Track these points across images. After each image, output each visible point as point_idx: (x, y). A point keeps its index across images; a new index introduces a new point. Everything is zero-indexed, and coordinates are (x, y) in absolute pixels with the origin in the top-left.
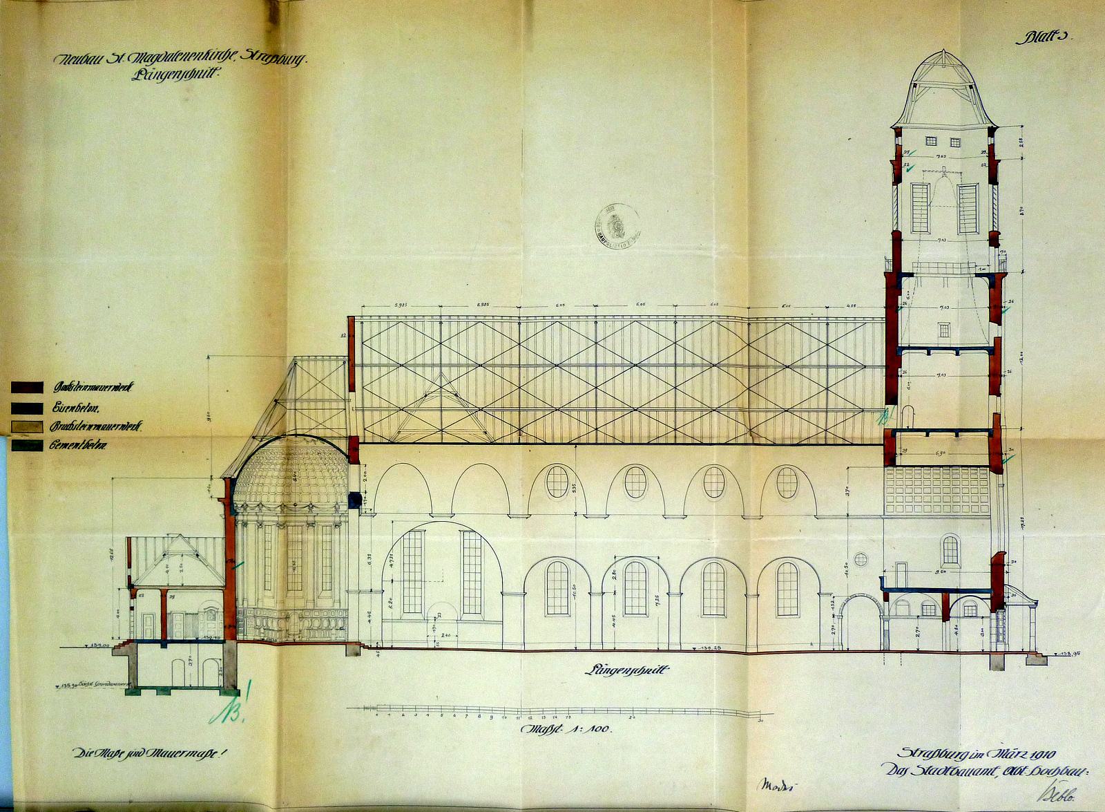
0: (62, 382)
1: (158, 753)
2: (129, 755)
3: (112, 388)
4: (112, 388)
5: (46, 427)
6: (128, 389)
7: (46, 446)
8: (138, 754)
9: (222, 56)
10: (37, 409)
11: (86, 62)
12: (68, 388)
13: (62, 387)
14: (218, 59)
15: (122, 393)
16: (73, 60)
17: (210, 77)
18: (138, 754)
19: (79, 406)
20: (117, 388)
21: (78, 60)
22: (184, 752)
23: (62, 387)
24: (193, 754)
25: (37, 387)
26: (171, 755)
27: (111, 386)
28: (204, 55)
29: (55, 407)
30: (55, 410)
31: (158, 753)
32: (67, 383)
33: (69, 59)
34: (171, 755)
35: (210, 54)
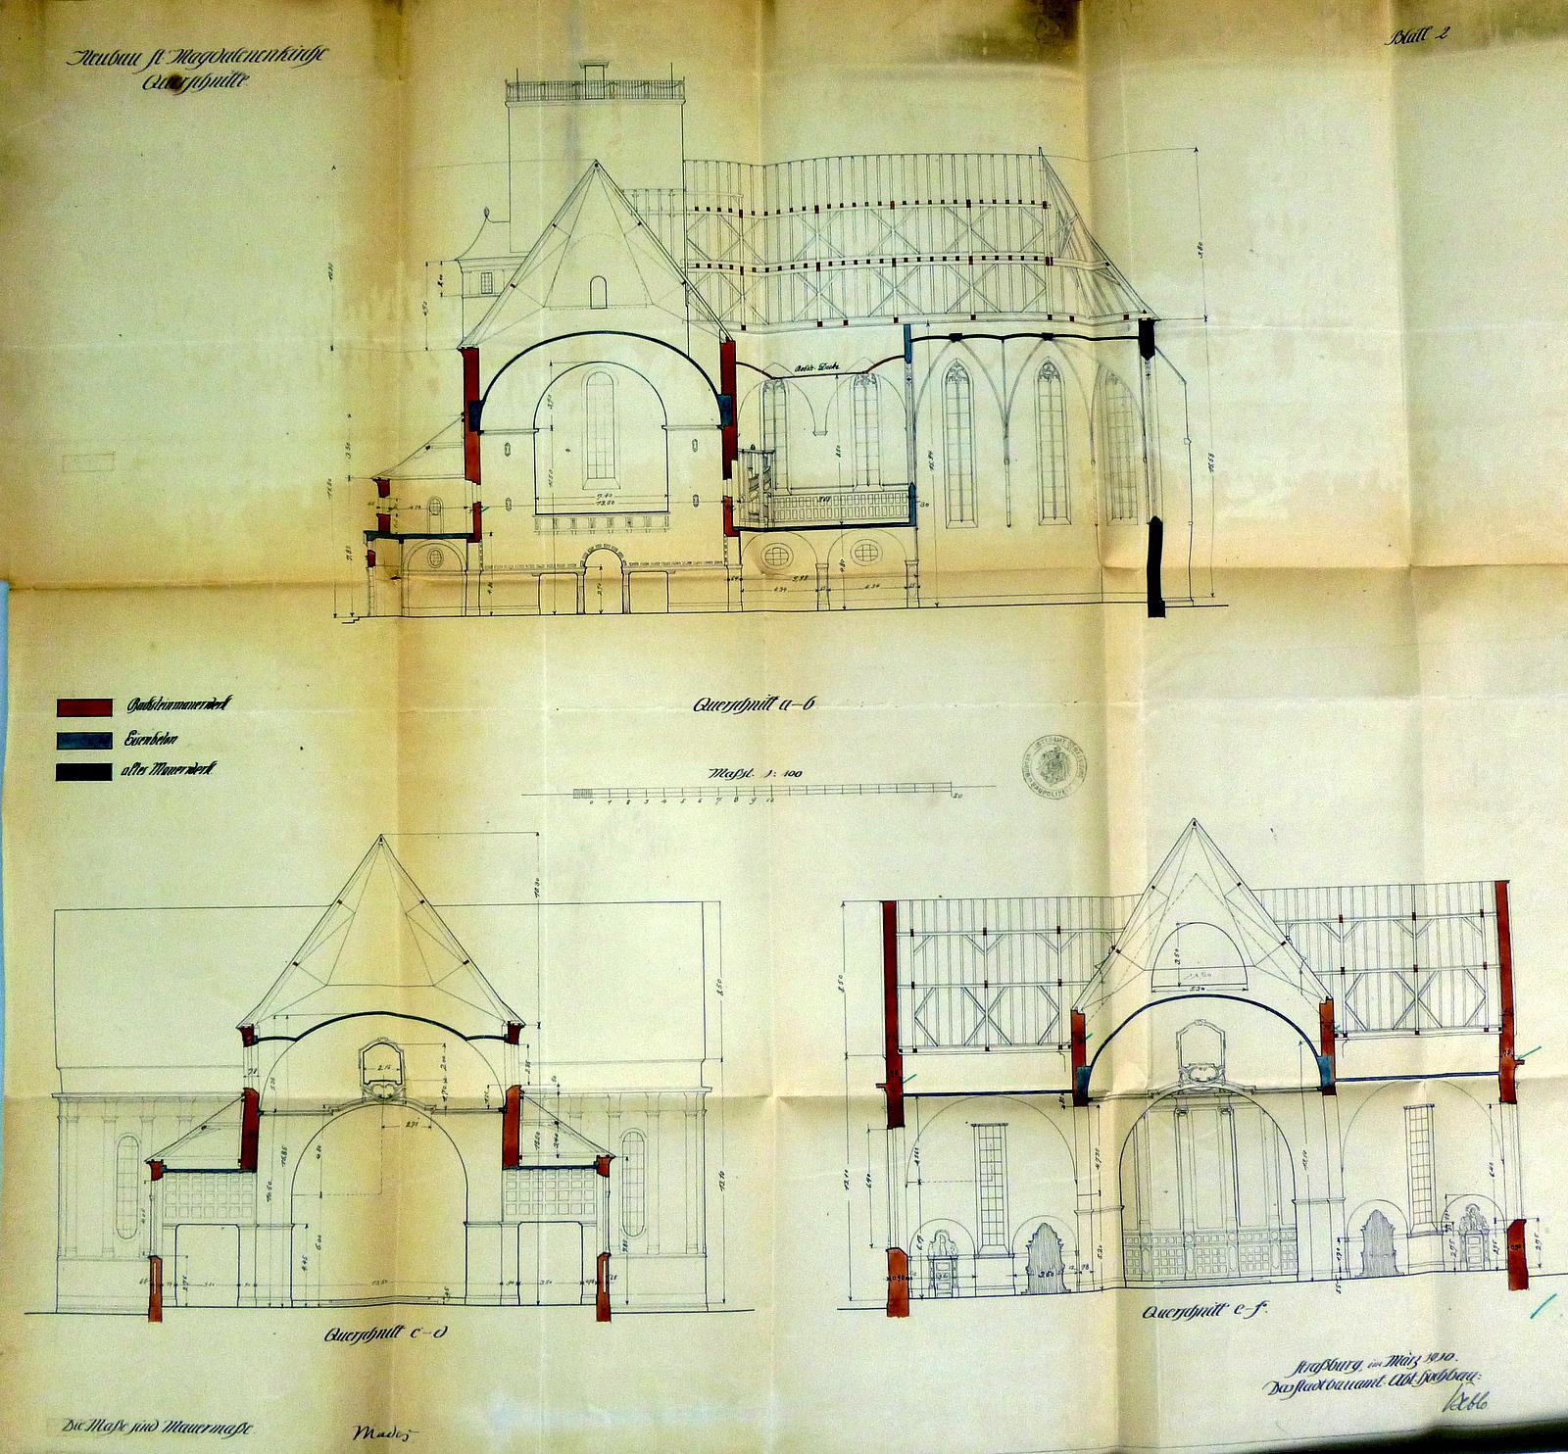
0: (139, 699)
1: (176, 1427)
2: (135, 1428)
3: (185, 771)
4: (185, 771)
5: (118, 740)
6: (207, 772)
7: (116, 772)
8: (148, 1428)
9: (198, 84)
10: (104, 741)
11: (117, 61)
12: (149, 706)
13: (138, 705)
14: (301, 59)
15: (216, 712)
16: (96, 58)
17: (1217, 1314)
18: (148, 1428)
19: (156, 737)
20: (192, 770)
21: (102, 60)
22: (209, 1426)
23: (138, 705)
24: (219, 1429)
25: (103, 707)
26: (193, 1429)
27: (185, 768)
28: (278, 54)
29: (128, 739)
30: (128, 743)
31: (176, 1427)
32: (145, 700)
33: (89, 57)
34: (193, 1429)
35: (290, 53)
